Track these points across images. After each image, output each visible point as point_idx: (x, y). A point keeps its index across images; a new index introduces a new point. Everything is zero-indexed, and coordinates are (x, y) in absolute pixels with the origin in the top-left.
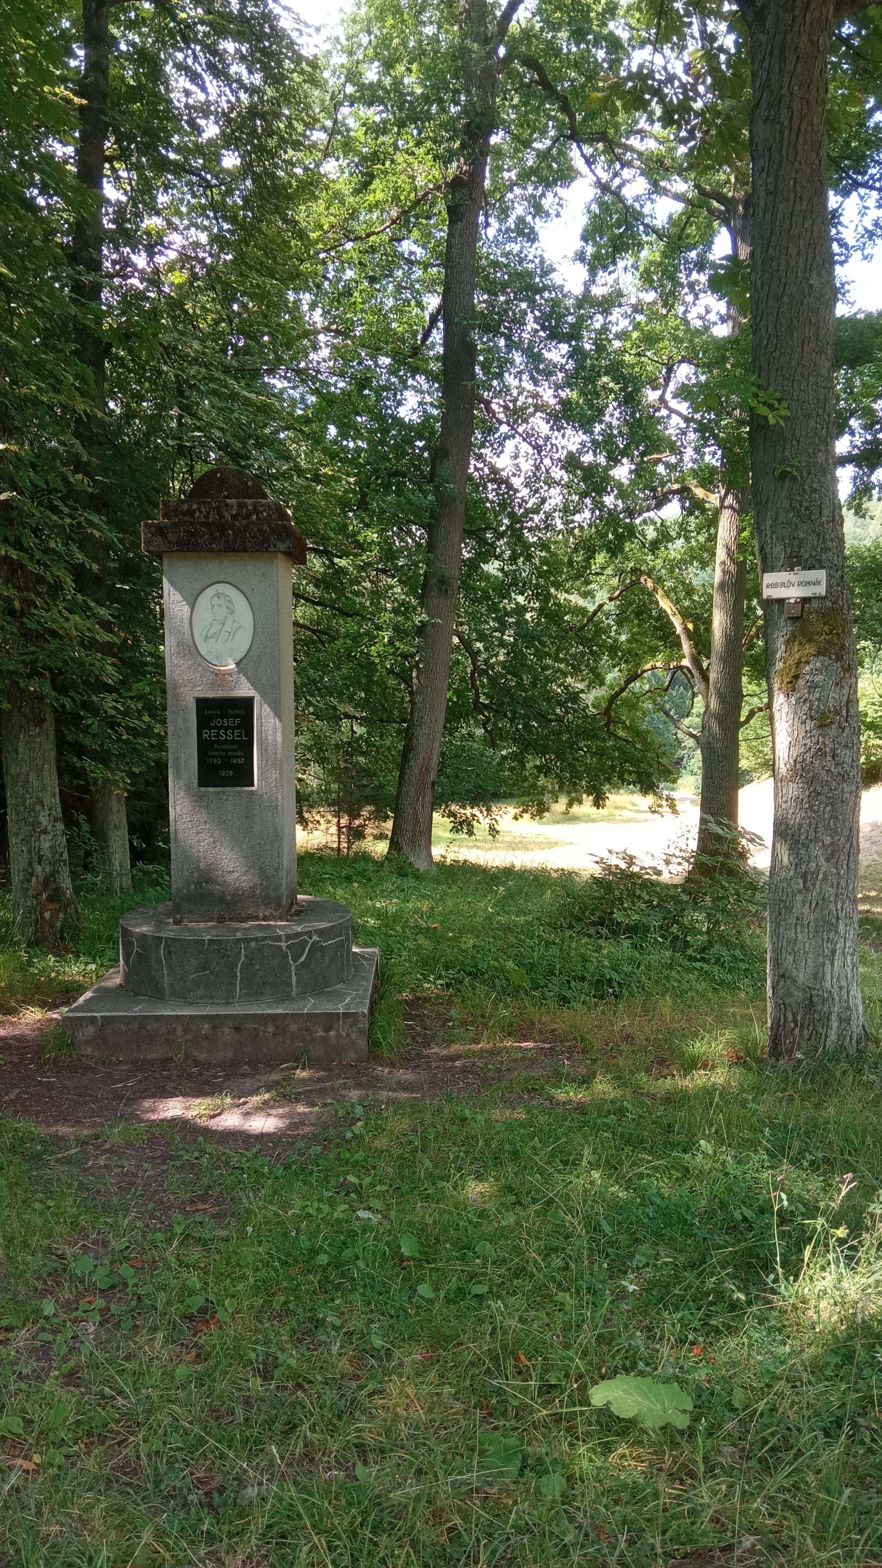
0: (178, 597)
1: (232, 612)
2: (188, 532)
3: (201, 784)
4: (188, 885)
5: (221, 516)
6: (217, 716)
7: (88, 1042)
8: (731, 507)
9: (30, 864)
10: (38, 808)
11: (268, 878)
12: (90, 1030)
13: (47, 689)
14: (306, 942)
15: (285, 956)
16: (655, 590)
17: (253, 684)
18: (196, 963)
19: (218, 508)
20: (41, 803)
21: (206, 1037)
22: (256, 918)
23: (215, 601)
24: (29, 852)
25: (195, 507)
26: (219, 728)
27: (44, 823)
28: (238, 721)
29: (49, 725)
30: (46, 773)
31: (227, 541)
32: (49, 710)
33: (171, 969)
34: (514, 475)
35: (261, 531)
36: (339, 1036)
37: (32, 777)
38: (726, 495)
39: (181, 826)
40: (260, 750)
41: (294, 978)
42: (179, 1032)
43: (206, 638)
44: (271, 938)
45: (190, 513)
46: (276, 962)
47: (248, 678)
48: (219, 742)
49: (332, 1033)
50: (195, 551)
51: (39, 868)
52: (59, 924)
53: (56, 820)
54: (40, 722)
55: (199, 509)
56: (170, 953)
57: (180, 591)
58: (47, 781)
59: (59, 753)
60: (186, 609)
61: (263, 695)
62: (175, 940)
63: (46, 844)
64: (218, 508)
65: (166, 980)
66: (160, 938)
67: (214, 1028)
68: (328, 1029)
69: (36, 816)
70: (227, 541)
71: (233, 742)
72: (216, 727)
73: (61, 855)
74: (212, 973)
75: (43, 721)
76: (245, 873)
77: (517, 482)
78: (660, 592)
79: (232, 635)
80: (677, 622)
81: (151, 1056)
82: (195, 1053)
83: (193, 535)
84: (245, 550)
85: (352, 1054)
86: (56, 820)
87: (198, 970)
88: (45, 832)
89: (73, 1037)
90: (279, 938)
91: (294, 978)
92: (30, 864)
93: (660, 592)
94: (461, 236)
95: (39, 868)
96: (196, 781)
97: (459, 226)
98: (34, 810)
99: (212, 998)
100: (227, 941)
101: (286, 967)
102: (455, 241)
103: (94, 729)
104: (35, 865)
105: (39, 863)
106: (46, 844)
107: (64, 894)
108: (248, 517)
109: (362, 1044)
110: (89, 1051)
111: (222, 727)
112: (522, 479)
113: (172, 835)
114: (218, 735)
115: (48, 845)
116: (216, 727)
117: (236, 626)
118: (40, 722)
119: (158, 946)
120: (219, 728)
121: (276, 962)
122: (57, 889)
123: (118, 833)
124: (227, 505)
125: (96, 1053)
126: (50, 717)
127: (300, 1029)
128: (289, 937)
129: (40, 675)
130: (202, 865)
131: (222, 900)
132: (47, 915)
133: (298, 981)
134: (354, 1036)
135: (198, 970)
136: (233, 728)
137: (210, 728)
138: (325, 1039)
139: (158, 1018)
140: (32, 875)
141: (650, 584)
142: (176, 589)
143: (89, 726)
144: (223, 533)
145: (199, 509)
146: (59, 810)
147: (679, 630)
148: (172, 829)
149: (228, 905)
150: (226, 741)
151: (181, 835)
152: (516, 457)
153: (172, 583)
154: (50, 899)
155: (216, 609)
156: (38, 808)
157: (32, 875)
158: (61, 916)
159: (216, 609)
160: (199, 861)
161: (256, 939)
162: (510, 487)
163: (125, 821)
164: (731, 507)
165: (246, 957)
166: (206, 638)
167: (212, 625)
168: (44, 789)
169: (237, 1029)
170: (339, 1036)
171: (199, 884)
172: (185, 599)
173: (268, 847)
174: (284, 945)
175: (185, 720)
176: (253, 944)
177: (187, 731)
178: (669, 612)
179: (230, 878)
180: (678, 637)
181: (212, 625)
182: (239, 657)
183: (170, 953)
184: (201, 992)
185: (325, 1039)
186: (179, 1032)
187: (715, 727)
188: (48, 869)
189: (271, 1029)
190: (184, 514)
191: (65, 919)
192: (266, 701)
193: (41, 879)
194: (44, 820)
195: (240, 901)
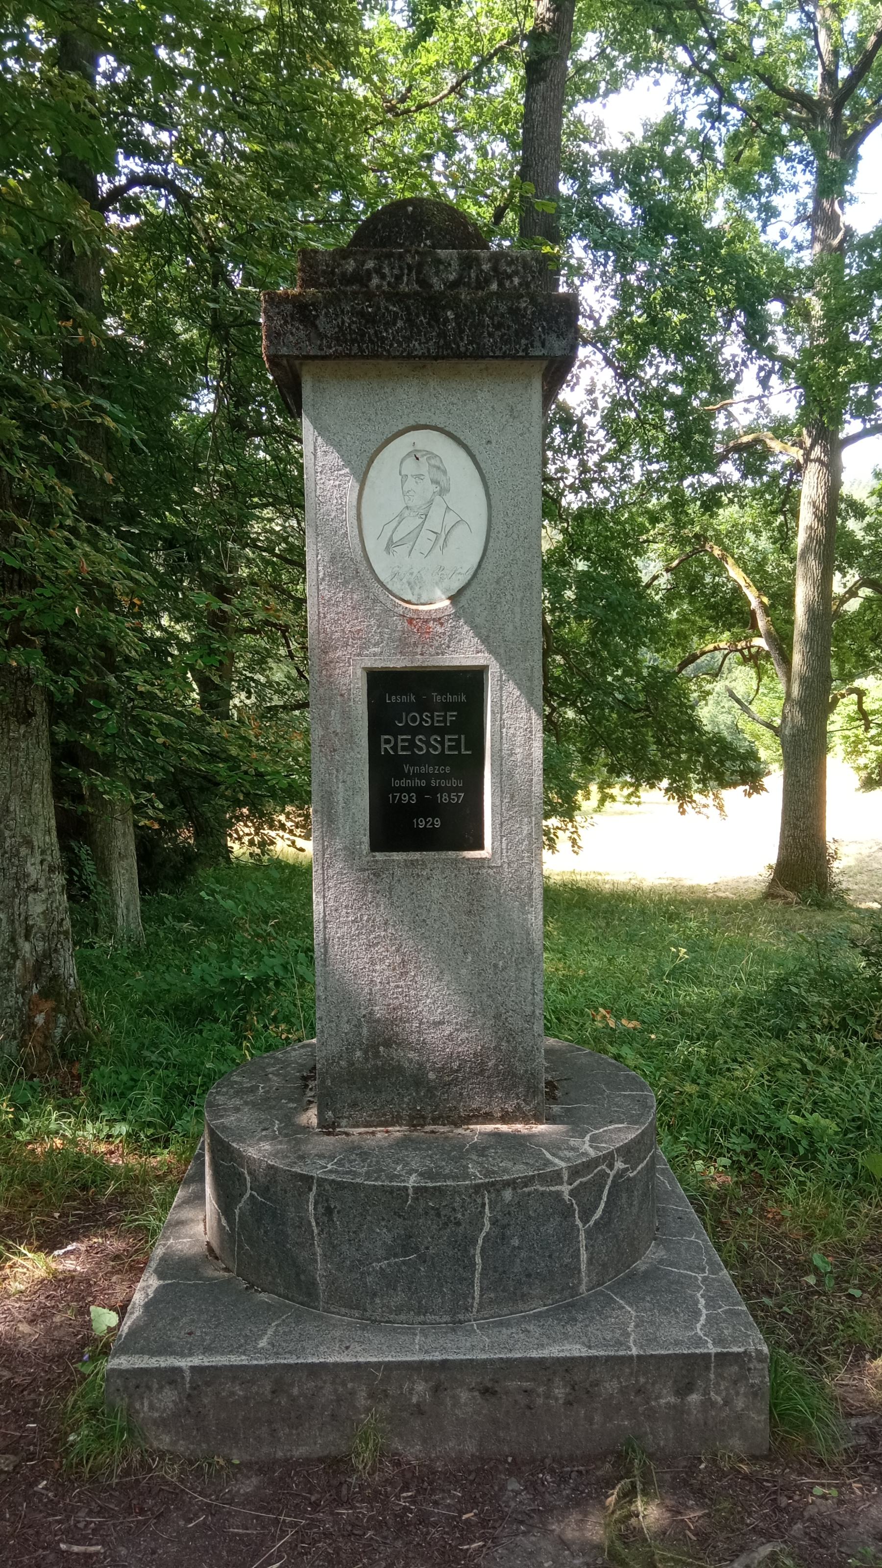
0: (333, 458)
1: (443, 491)
2: (362, 314)
3: (375, 846)
4: (350, 1051)
5: (423, 283)
6: (409, 707)
7: (163, 1423)
8: (818, 460)
9: (13, 940)
10: (24, 851)
11: (510, 1035)
12: (168, 1398)
13: (38, 664)
14: (604, 1175)
15: (567, 1213)
16: (724, 558)
17: (485, 640)
18: (388, 1238)
19: (420, 265)
20: (28, 843)
21: (419, 1410)
22: (488, 1118)
23: (410, 466)
24: (11, 922)
25: (370, 264)
26: (415, 731)
27: (34, 876)
28: (452, 716)
29: (39, 721)
30: (36, 797)
31: (442, 334)
32: (40, 698)
33: (332, 1247)
34: (589, 413)
35: (514, 312)
36: (708, 1404)
37: (14, 804)
38: (812, 446)
39: (335, 931)
40: (498, 774)
41: (584, 1256)
42: (362, 1399)
43: (390, 546)
44: (544, 1179)
45: (360, 278)
46: (550, 1228)
47: (475, 627)
48: (415, 760)
49: (694, 1398)
50: (375, 356)
51: (27, 947)
52: (58, 1032)
53: (52, 870)
54: (26, 717)
55: (378, 271)
56: (329, 1211)
57: (338, 446)
58: (38, 809)
59: (56, 762)
60: (351, 485)
61: (506, 662)
62: (340, 1186)
63: (37, 907)
64: (420, 265)
65: (320, 1270)
66: (307, 1180)
67: (436, 1390)
68: (684, 1389)
69: (22, 865)
70: (442, 334)
71: (442, 759)
72: (407, 729)
73: (60, 924)
74: (423, 1259)
75: (31, 715)
76: (466, 1026)
77: (591, 422)
78: (730, 560)
79: (442, 538)
80: (751, 594)
81: (300, 1452)
82: (397, 1445)
83: (371, 320)
84: (478, 355)
85: (736, 1443)
86: (52, 870)
87: (391, 1252)
88: (35, 889)
89: (131, 1412)
90: (556, 1179)
91: (584, 1256)
92: (13, 940)
93: (730, 560)
94: (544, 99)
95: (27, 947)
96: (366, 839)
97: (542, 86)
98: (17, 854)
99: (422, 1310)
100: (456, 1191)
101: (569, 1236)
102: (535, 106)
103: (112, 727)
104: (21, 941)
105: (27, 938)
106: (37, 907)
107: (66, 985)
108: (482, 283)
109: (759, 1419)
110: (164, 1441)
111: (420, 729)
112: (598, 418)
113: (318, 953)
114: (412, 745)
115: (40, 909)
116: (407, 729)
117: (451, 519)
118: (26, 717)
119: (302, 1194)
120: (415, 731)
121: (550, 1228)
122: (55, 978)
123: (124, 863)
124: (438, 261)
125: (181, 1447)
126: (40, 709)
127: (623, 1391)
128: (575, 1172)
129: (27, 643)
130: (379, 1012)
131: (418, 1080)
132: (40, 1019)
133: (590, 1261)
134: (740, 1403)
135: (391, 1252)
136: (442, 732)
137: (396, 732)
138: (679, 1412)
139: (314, 1370)
140: (15, 957)
141: (717, 552)
142: (329, 441)
143: (103, 722)
144: (435, 318)
145: (378, 271)
146: (57, 853)
147: (754, 604)
148: (318, 938)
149: (431, 1090)
150: (427, 759)
151: (334, 950)
152: (590, 392)
153: (321, 429)
154: (45, 994)
155: (410, 483)
156: (24, 851)
157: (15, 957)
158: (62, 1019)
159: (410, 483)
160: (371, 1002)
161: (512, 1184)
162: (582, 428)
163: (132, 847)
164: (818, 460)
165: (494, 1222)
166: (390, 546)
167: (401, 518)
168: (33, 821)
169: (487, 1392)
170: (708, 1404)
171: (372, 1048)
172: (348, 463)
173: (512, 972)
174: (565, 1189)
175: (346, 715)
176: (508, 1194)
177: (351, 737)
178: (742, 584)
179: (433, 1036)
180: (753, 613)
181: (401, 518)
182: (456, 585)
183: (329, 1211)
184: (399, 1298)
185: (679, 1412)
186: (362, 1399)
187: (798, 717)
188: (41, 946)
189: (560, 1392)
190: (347, 279)
191: (68, 1025)
192: (511, 675)
193: (31, 963)
194: (33, 870)
195: (455, 1082)
